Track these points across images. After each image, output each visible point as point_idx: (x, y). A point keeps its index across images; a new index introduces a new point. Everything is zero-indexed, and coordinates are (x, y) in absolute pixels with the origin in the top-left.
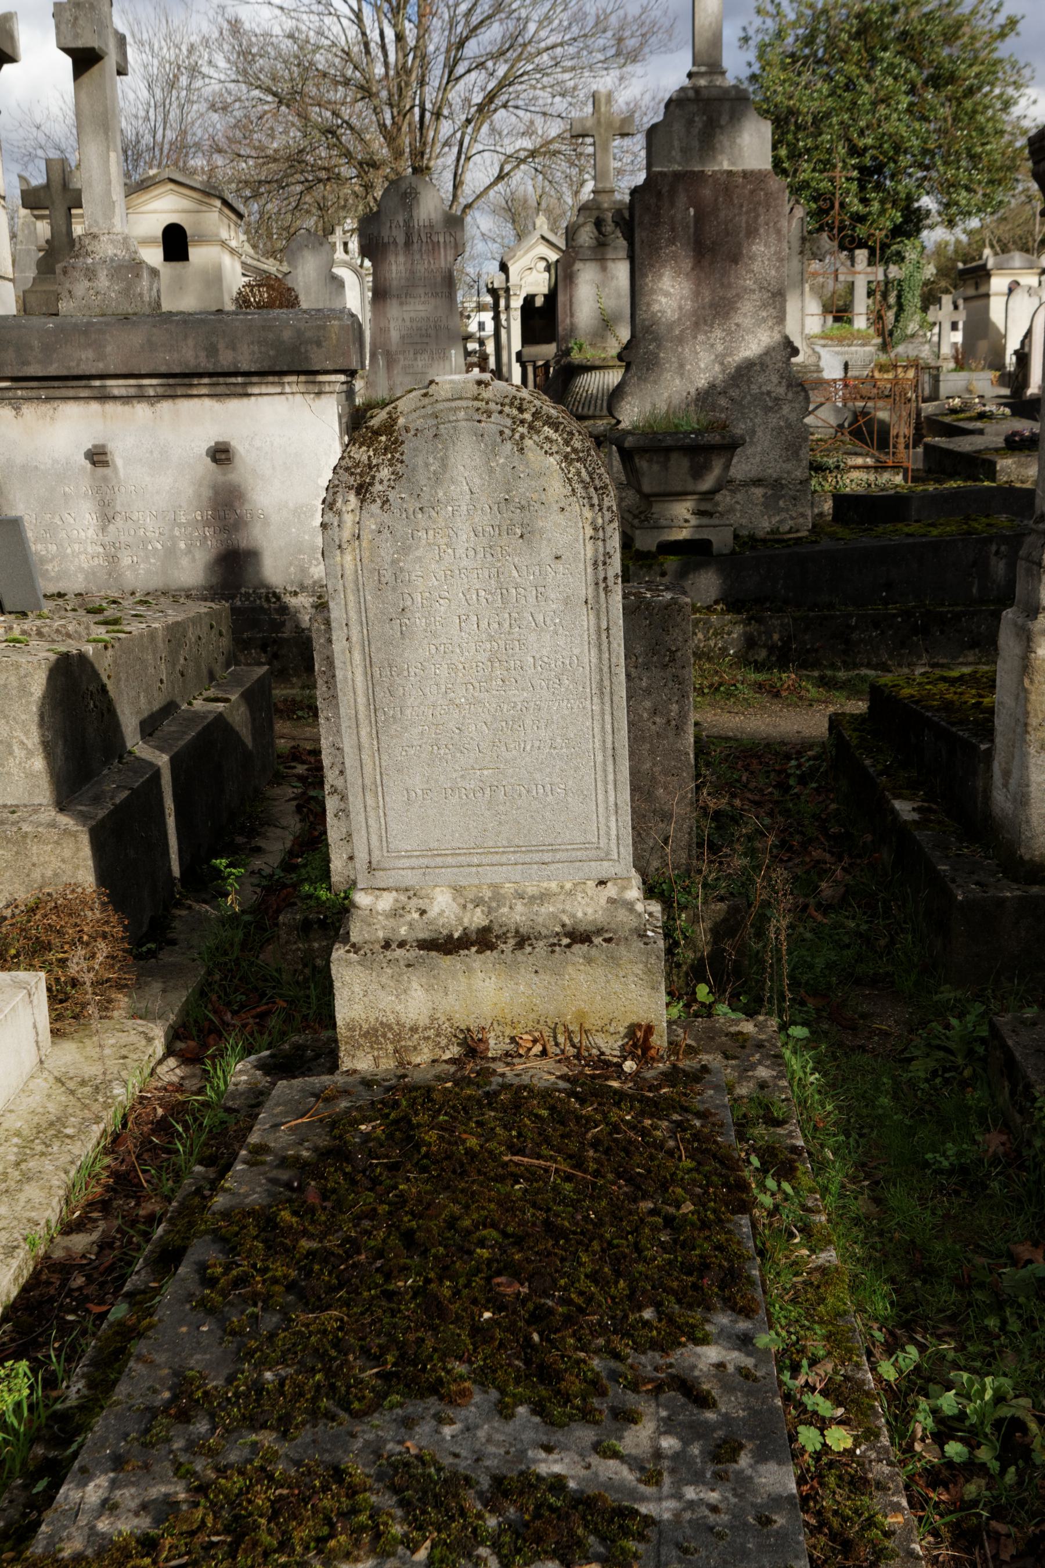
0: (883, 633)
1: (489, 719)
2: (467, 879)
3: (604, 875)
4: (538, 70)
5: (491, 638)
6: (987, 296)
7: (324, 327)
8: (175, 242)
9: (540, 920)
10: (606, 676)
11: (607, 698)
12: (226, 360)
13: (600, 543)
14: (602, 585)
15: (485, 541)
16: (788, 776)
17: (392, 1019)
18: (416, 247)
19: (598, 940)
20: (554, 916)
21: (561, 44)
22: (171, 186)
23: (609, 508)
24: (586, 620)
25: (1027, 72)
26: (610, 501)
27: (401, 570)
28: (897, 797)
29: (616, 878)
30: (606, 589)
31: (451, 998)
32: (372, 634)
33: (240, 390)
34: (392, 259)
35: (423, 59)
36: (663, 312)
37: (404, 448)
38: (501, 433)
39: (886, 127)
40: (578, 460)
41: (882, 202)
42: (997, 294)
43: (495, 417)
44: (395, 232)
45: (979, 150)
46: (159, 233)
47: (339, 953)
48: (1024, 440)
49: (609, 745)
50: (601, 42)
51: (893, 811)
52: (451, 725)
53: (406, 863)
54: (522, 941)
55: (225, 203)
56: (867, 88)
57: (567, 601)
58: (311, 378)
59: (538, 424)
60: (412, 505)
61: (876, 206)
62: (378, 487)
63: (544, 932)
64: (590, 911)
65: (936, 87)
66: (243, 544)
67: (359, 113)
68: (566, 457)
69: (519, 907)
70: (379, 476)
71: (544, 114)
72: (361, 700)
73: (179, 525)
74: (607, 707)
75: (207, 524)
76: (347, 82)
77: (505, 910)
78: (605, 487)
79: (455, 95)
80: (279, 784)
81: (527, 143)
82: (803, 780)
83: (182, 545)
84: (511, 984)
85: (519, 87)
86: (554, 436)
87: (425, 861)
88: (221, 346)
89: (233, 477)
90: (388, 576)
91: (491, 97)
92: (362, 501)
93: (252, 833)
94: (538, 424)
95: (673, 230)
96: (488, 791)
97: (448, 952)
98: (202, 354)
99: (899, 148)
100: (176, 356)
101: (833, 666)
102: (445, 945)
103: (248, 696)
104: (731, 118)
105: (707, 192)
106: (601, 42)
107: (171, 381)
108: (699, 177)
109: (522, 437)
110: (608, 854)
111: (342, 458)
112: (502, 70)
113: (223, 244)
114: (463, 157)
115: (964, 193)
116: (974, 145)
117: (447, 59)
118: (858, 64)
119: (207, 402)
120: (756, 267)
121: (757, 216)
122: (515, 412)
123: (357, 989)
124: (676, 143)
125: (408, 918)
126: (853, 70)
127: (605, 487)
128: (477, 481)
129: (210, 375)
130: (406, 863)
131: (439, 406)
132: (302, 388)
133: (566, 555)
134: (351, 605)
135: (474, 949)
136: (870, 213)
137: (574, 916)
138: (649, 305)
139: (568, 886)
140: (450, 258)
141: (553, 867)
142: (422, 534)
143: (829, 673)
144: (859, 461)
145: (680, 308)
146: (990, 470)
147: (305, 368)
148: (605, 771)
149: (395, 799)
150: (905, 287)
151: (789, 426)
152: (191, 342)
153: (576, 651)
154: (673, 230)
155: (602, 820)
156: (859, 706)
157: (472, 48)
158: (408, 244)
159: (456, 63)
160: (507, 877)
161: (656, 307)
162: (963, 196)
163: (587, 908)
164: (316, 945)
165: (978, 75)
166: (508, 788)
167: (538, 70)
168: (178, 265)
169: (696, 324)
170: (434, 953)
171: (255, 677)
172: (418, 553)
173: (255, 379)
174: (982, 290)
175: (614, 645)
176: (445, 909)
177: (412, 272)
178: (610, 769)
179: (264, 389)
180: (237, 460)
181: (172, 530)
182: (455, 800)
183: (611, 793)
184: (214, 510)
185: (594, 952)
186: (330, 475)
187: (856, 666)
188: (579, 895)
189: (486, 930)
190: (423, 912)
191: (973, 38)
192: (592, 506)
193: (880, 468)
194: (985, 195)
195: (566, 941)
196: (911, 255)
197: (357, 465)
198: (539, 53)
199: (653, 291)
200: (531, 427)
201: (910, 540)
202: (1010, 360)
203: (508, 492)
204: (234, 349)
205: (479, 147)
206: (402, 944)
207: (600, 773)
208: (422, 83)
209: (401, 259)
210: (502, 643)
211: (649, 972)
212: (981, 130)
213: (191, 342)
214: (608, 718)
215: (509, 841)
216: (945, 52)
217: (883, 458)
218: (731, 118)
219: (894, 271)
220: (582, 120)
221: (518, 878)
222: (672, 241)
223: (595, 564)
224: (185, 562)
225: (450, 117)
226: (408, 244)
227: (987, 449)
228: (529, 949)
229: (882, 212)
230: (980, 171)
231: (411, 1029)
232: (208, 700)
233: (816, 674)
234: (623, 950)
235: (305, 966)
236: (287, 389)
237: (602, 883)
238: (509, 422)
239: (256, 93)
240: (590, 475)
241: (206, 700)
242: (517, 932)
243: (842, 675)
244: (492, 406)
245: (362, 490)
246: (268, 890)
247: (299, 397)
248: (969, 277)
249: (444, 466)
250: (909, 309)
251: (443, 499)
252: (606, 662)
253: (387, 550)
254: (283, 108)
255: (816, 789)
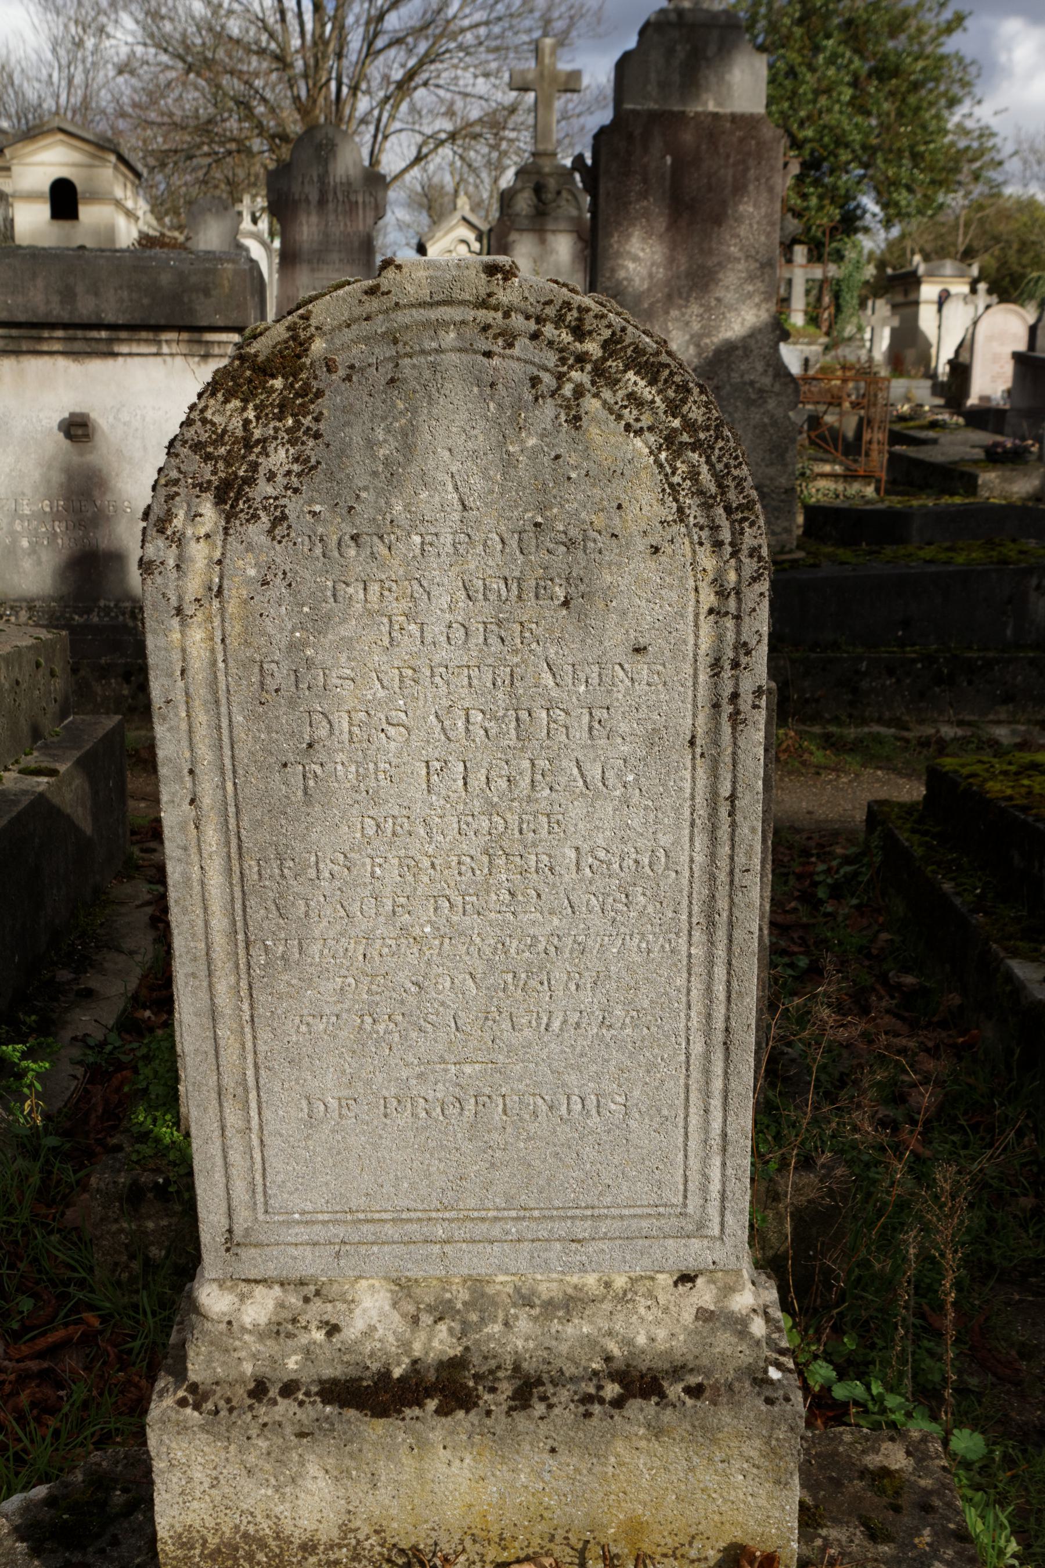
0: (898, 681)
1: (480, 967)
2: (424, 1268)
3: (690, 1265)
4: (460, 47)
5: (491, 809)
6: (916, 303)
7: (214, 271)
8: (64, 199)
9: (564, 1348)
10: (722, 891)
11: (721, 934)
12: (86, 307)
13: (729, 623)
14: (726, 709)
15: (488, 609)
16: (815, 884)
17: (266, 1528)
18: (331, 206)
19: (675, 1391)
20: (591, 1342)
21: (487, 23)
22: (61, 136)
23: (754, 552)
24: (688, 779)
25: (973, 70)
26: (756, 537)
27: (309, 663)
28: (1015, 954)
29: (711, 1272)
30: (735, 718)
31: (384, 1494)
32: (245, 793)
33: (103, 347)
34: (303, 218)
35: (340, 28)
36: (630, 280)
37: (323, 405)
38: (535, 381)
39: (826, 118)
40: (695, 446)
41: (821, 197)
42: (927, 302)
43: (522, 346)
44: (307, 189)
45: (922, 148)
46: (46, 187)
47: (162, 1407)
48: (1006, 452)
49: (719, 1024)
50: (528, 23)
51: (1009, 977)
52: (403, 977)
53: (303, 1233)
54: (528, 1389)
55: (121, 158)
56: (809, 76)
57: (653, 739)
58: (196, 336)
59: (614, 365)
60: (336, 529)
61: (814, 201)
62: (264, 489)
63: (570, 1370)
64: (661, 1334)
65: (881, 80)
66: (104, 544)
67: (270, 85)
68: (670, 439)
69: (523, 1325)
70: (266, 464)
71: (466, 95)
72: (219, 923)
73: (22, 518)
74: (721, 952)
75: (56, 516)
76: (262, 52)
77: (495, 1328)
78: (749, 506)
79: (375, 70)
80: (131, 878)
81: (448, 126)
82: (837, 892)
83: (25, 543)
84: (503, 1472)
85: (439, 66)
86: (647, 393)
87: (341, 1231)
88: (80, 289)
89: (91, 458)
90: (281, 676)
91: (411, 75)
92: (230, 516)
93: (83, 963)
94: (614, 365)
95: (645, 181)
96: (470, 1105)
97: (381, 1412)
98: (55, 299)
99: (841, 142)
100: (20, 299)
101: (836, 720)
102: (374, 1394)
103: (86, 764)
104: (720, 50)
105: (688, 137)
106: (528, 23)
107: (14, 332)
108: (681, 117)
109: (579, 392)
110: (701, 1225)
111: (187, 423)
112: (422, 47)
113: (118, 204)
114: (381, 135)
115: (904, 193)
116: (917, 144)
117: (367, 31)
118: (799, 51)
119: (61, 362)
120: (743, 231)
121: (746, 170)
122: (566, 337)
123: (198, 1474)
124: (653, 76)
125: (304, 1339)
126: (794, 57)
127: (749, 506)
128: (477, 482)
129: (65, 326)
130: (303, 1233)
131: (403, 317)
132: (184, 348)
133: (657, 644)
134: (202, 732)
135: (432, 1404)
136: (807, 208)
137: (629, 1342)
138: (613, 270)
139: (620, 1282)
140: (370, 221)
141: (591, 1248)
142: (355, 590)
143: (832, 729)
144: (827, 468)
145: (651, 276)
146: (970, 484)
147: (187, 322)
148: (707, 1072)
149: (283, 1115)
150: (844, 287)
151: (774, 423)
152: (40, 283)
153: (665, 840)
154: (645, 181)
155: (694, 1163)
156: (911, 791)
157: (393, 21)
158: (322, 202)
159: (376, 35)
160: (503, 1269)
161: (622, 274)
162: (902, 197)
163: (656, 1328)
164: (150, 1225)
165: (923, 70)
166: (513, 1100)
167: (460, 47)
168: (66, 225)
169: (669, 297)
170: (352, 1413)
171: (101, 733)
172: (347, 630)
173: (123, 335)
174: (912, 297)
175: (744, 830)
176: (374, 1322)
177: (326, 235)
178: (718, 1068)
179: (135, 349)
180: (98, 437)
181: (11, 523)
182: (403, 1119)
183: (717, 1115)
184: (67, 499)
185: (668, 1416)
186: (161, 459)
187: (864, 722)
188: (642, 1302)
189: (455, 1365)
190: (333, 1330)
191: (920, 31)
192: (718, 544)
193: (849, 477)
194: (925, 196)
195: (612, 1390)
196: (850, 254)
197: (220, 439)
198: (463, 30)
199: (618, 254)
200: (599, 372)
201: (933, 568)
202: (943, 369)
203: (542, 508)
204: (97, 294)
205: (397, 125)
206: (289, 1389)
207: (696, 1074)
208: (339, 56)
209: (314, 219)
210: (513, 819)
211: (772, 1452)
212: (924, 127)
213: (40, 283)
214: (720, 972)
215: (509, 1198)
216: (891, 44)
217: (854, 466)
218: (720, 50)
219: (833, 270)
220: (523, 72)
221: (523, 1265)
222: (644, 195)
223: (716, 665)
224: (27, 564)
225: (368, 92)
226: (322, 202)
227: (962, 460)
228: (540, 1408)
229: (820, 208)
230: (922, 171)
231: (303, 1547)
232: (26, 772)
233: (817, 729)
234: (725, 1415)
235: (132, 1257)
236: (165, 349)
237: (686, 1278)
238: (551, 359)
239: (164, 58)
240: (719, 479)
241: (23, 771)
242: (517, 1368)
243: (852, 732)
244: (517, 321)
245: (230, 494)
246: (96, 1074)
247: (179, 361)
248: (898, 285)
249: (408, 449)
250: (847, 311)
251: (403, 519)
252: (723, 863)
253: (280, 622)
254: (192, 76)
255: (857, 907)
